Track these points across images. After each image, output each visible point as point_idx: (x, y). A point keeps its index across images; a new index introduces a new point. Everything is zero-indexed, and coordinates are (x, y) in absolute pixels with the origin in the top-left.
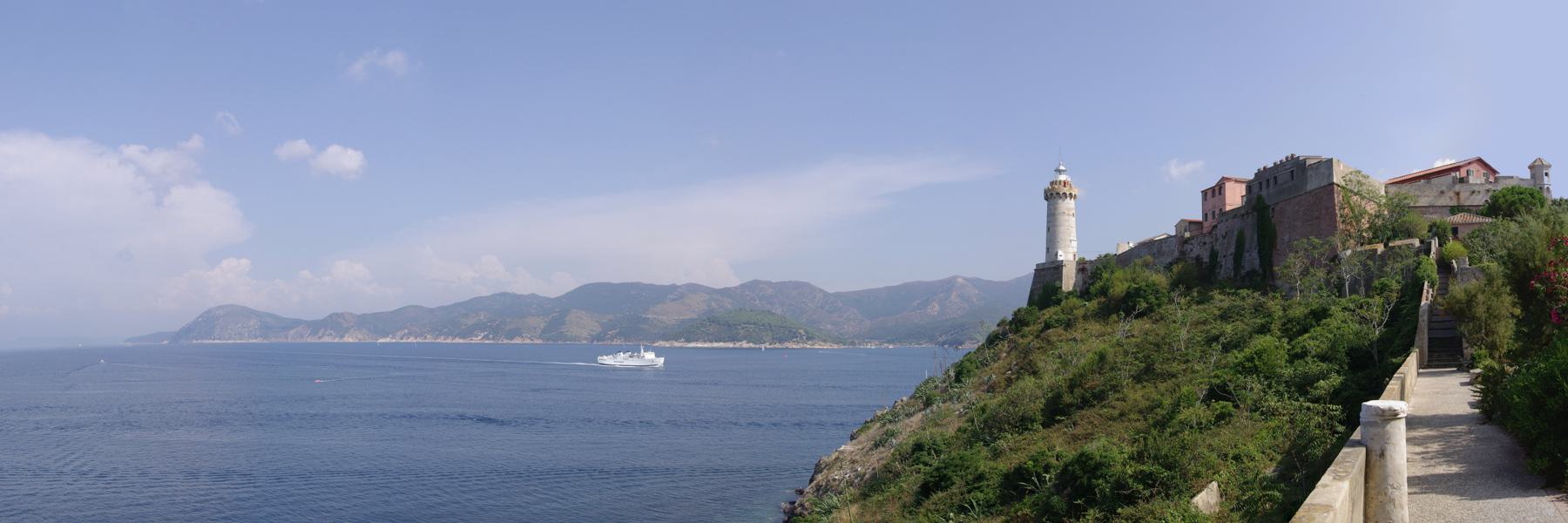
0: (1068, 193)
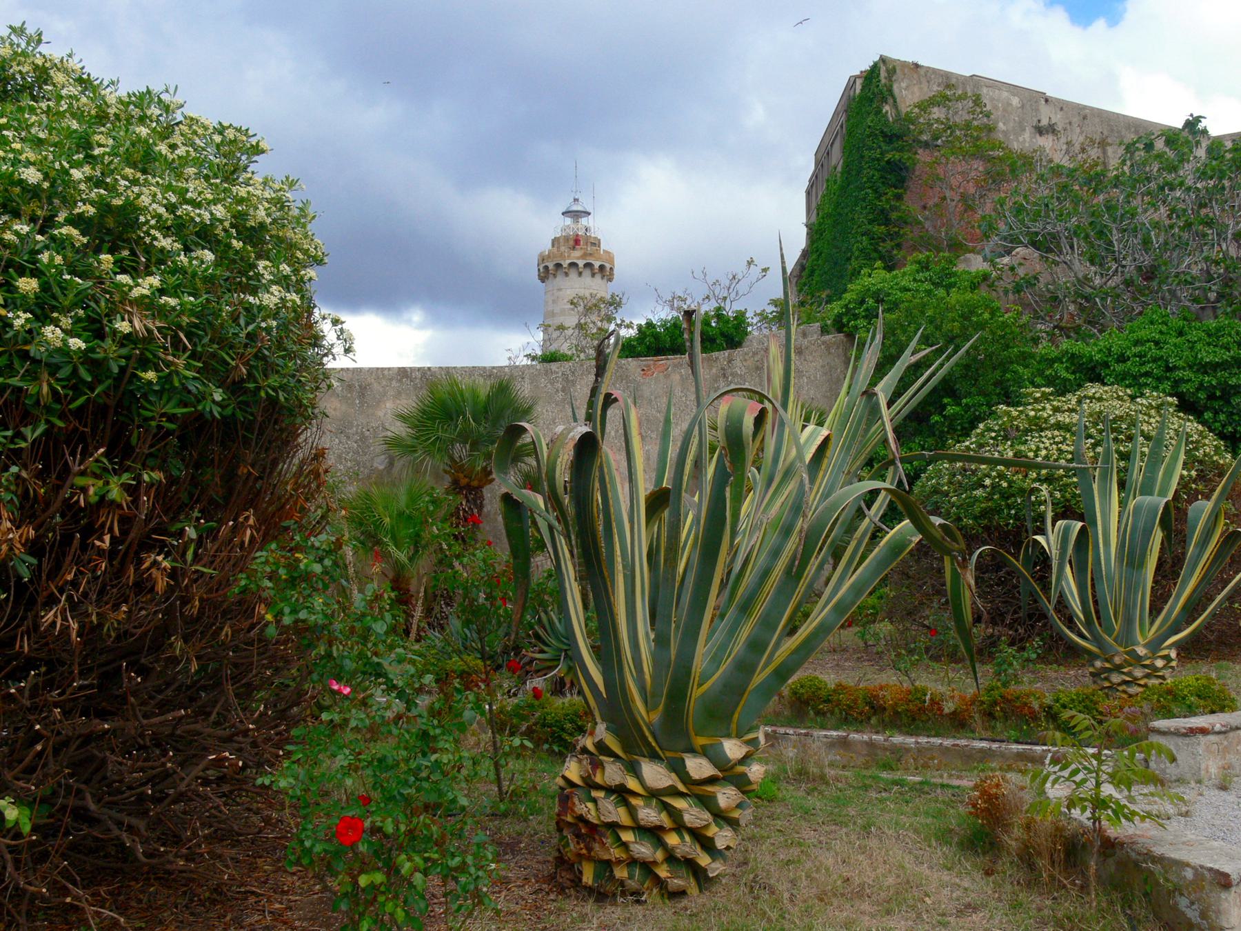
0: (581, 263)
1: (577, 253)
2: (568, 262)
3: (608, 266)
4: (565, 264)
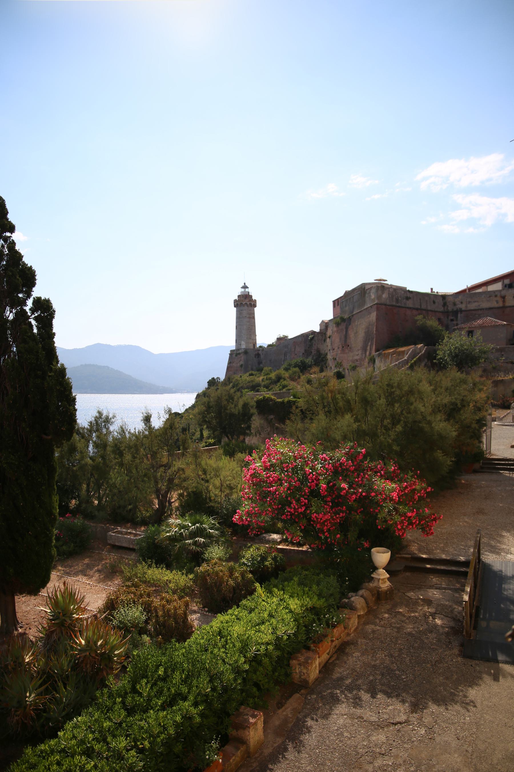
0: (248, 303)
1: (247, 300)
2: (244, 303)
3: (253, 303)
4: (244, 303)
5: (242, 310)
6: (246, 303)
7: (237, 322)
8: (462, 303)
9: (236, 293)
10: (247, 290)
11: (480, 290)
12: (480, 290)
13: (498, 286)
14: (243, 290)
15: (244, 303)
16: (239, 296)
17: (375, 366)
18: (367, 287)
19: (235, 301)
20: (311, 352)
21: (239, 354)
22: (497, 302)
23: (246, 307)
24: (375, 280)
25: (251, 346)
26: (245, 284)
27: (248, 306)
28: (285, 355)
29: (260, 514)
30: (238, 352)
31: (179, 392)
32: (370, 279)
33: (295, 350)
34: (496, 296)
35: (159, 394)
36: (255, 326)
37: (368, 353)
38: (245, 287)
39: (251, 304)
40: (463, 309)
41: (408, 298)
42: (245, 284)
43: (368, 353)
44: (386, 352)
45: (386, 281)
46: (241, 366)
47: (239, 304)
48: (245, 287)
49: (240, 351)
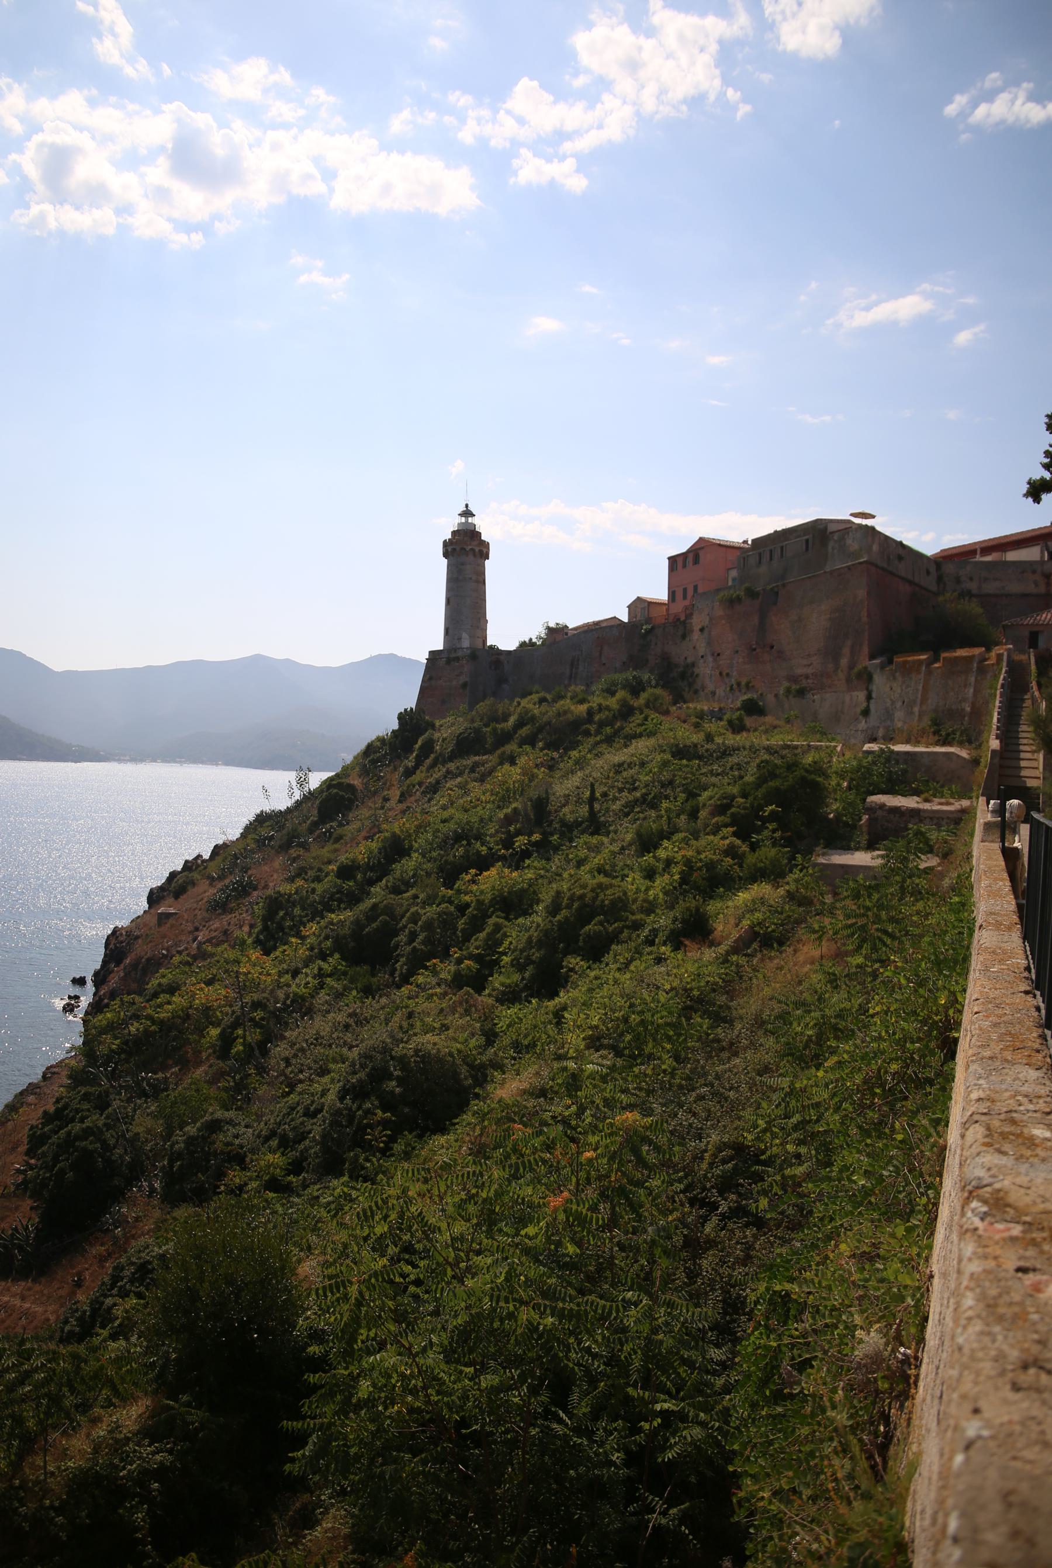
0: (477, 549)
4: (468, 548)
5: (462, 564)
6: (472, 550)
7: (449, 590)
8: (971, 579)
9: (448, 525)
10: (470, 520)
11: (1012, 556)
12: (1012, 556)
13: (1032, 554)
14: (463, 520)
15: (468, 548)
16: (454, 533)
17: (874, 688)
18: (832, 528)
19: (446, 544)
20: (647, 661)
21: (457, 659)
22: (1036, 584)
23: (471, 558)
24: (852, 515)
25: (480, 646)
26: (467, 506)
27: (475, 555)
28: (572, 665)
29: (125, 1023)
30: (453, 655)
31: (115, 760)
32: (838, 511)
33: (600, 655)
34: (1034, 572)
35: (72, 761)
36: (485, 600)
37: (844, 662)
38: (467, 513)
39: (481, 551)
40: (974, 592)
41: (900, 558)
42: (467, 506)
43: (844, 662)
44: (909, 659)
45: (873, 517)
46: (465, 685)
47: (458, 548)
48: (467, 513)
49: (460, 654)
